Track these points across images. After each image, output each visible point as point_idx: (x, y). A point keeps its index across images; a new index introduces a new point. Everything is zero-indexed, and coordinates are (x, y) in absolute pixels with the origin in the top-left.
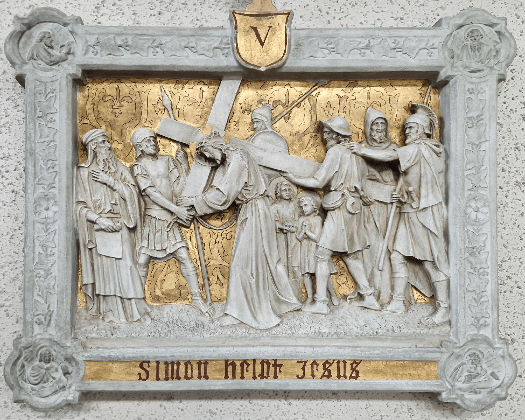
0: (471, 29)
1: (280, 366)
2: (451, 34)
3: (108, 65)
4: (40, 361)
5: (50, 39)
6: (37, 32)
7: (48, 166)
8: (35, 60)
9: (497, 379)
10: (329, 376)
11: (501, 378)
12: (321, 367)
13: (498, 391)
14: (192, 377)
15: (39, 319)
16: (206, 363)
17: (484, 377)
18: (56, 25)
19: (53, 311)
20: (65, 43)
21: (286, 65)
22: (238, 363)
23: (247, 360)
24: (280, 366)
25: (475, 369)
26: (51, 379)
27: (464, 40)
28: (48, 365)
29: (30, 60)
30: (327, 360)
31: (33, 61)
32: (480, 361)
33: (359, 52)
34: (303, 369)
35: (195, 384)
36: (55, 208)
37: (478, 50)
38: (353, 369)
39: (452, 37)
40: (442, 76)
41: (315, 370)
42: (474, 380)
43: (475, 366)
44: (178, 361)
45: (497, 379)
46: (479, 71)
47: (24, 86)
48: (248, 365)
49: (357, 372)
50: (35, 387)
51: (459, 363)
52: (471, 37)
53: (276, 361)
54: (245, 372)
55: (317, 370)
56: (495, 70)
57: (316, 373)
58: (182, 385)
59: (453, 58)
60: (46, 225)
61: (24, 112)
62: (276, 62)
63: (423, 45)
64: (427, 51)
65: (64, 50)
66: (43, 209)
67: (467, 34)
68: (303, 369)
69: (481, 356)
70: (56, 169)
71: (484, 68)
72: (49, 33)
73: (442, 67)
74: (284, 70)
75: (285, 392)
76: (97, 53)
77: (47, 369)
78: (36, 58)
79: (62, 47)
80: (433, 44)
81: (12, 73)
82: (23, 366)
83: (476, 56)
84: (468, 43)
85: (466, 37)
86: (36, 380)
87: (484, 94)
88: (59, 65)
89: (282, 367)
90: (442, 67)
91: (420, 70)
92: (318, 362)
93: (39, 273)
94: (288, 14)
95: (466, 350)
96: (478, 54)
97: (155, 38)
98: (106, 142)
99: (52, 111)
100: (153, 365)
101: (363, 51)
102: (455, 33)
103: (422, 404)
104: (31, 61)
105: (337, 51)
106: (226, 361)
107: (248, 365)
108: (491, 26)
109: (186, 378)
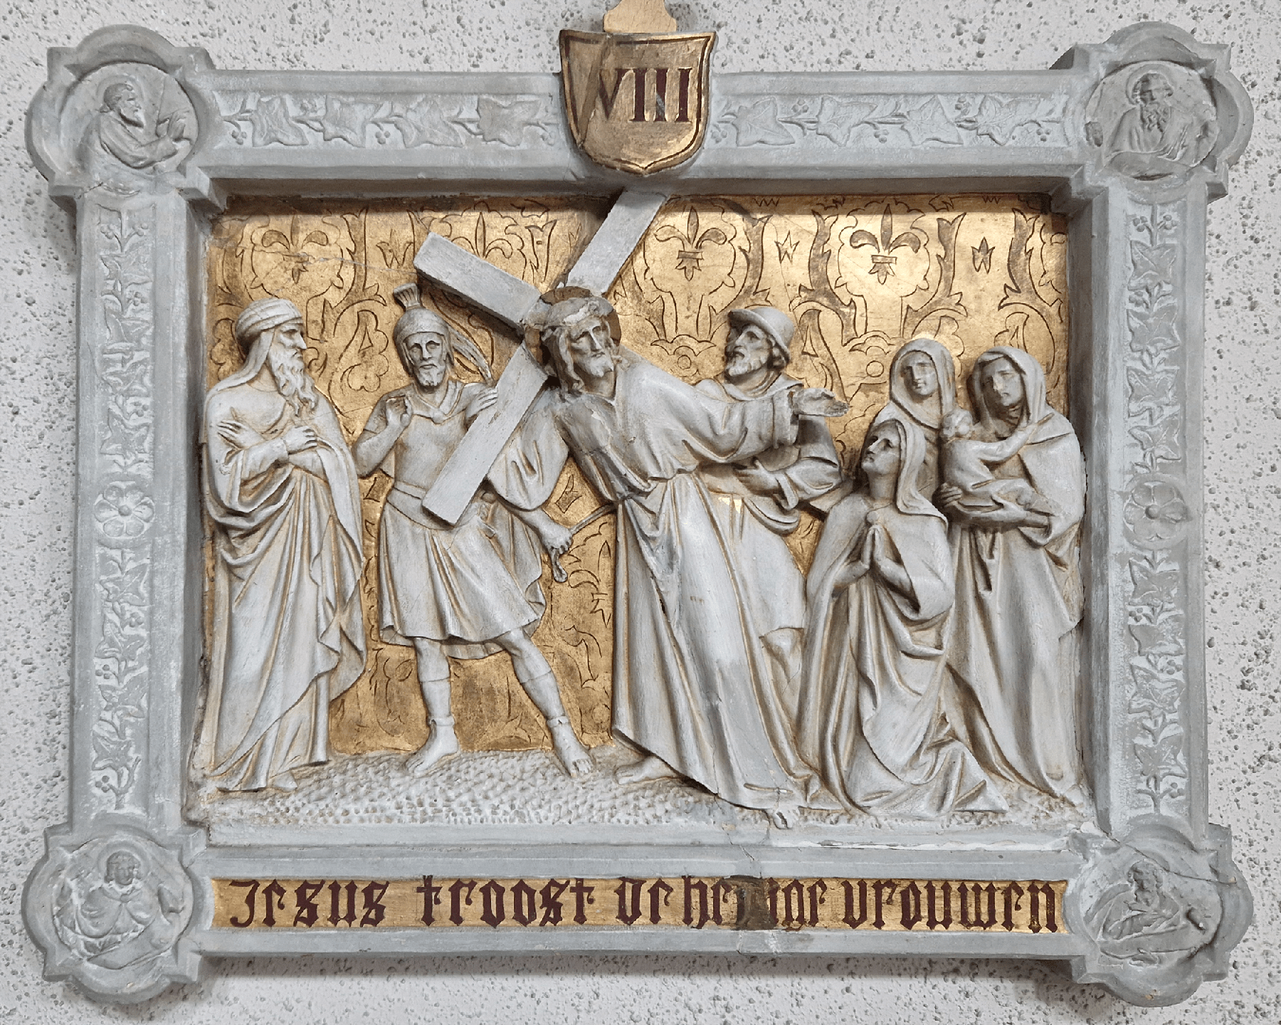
1: (590, 889)
3: (1007, 167)
4: (107, 880)
10: (311, 920)
14: (637, 913)
15: (105, 779)
17: (1170, 921)
21: (701, 160)
23: (802, 879)
24: (590, 889)
27: (1126, 101)
28: (125, 890)
30: (1014, 882)
34: (250, 900)
35: (564, 937)
38: (369, 904)
41: (662, 902)
44: (352, 882)
48: (1020, 893)
49: (380, 911)
53: (428, 880)
54: (463, 904)
55: (667, 903)
56: (1105, 52)
57: (276, 912)
59: (1099, 145)
64: (1036, 127)
68: (250, 900)
75: (848, 960)
77: (124, 899)
79: (159, 122)
80: (1051, 111)
89: (593, 893)
92: (284, 886)
93: (106, 668)
98: (297, 335)
103: (1008, 986)
107: (1020, 893)
108: (1190, 65)
109: (978, 922)
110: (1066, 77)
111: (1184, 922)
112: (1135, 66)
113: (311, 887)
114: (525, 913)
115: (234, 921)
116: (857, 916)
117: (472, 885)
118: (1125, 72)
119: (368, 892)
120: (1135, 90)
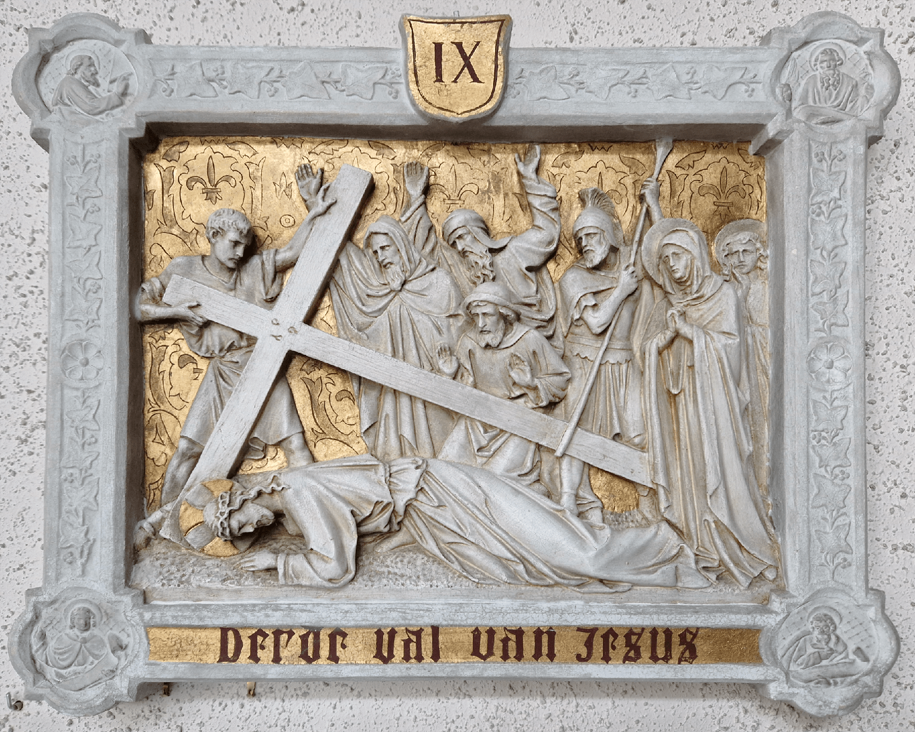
0: (821, 49)
2: (788, 58)
5: (92, 69)
6: (61, 63)
7: (88, 288)
8: (66, 105)
9: (866, 660)
11: (872, 658)
12: (621, 641)
13: (868, 680)
14: (490, 652)
16: (551, 634)
18: (100, 43)
19: (95, 540)
20: (118, 74)
21: (501, 113)
22: (245, 635)
25: (827, 643)
26: (91, 659)
28: (86, 634)
29: (56, 104)
31: (63, 107)
32: (835, 628)
33: (388, 89)
36: (98, 363)
37: (833, 85)
39: (790, 63)
40: (771, 130)
41: (338, 646)
42: (824, 662)
43: (826, 636)
45: (866, 660)
46: (838, 121)
47: (47, 150)
50: (63, 672)
51: (798, 633)
52: (822, 62)
58: (596, 670)
60: (84, 393)
61: (895, 677)
62: (480, 106)
63: (737, 76)
65: (117, 88)
66: (78, 363)
67: (813, 59)
68: (589, 644)
69: (836, 620)
70: (101, 294)
71: (845, 117)
72: (90, 58)
73: (771, 116)
74: (497, 122)
76: (172, 91)
78: (67, 101)
79: (112, 82)
81: (25, 124)
82: (43, 636)
83: (830, 96)
84: (817, 73)
85: (813, 63)
86: (63, 660)
87: (844, 162)
88: (107, 115)
90: (771, 116)
91: (734, 122)
94: (502, 21)
95: (810, 610)
96: (834, 93)
97: (628, 68)
99: (94, 194)
100: (647, 636)
101: (633, 86)
102: (795, 54)
104: (56, 107)
105: (588, 87)
106: (591, 631)
110: (54, 137)
111: (852, 657)
112: (817, 43)
113: (635, 634)
114: (310, 654)
115: (579, 658)
116: (483, 651)
117: (291, 634)
118: (811, 47)
119: (682, 637)
120: (816, 61)
